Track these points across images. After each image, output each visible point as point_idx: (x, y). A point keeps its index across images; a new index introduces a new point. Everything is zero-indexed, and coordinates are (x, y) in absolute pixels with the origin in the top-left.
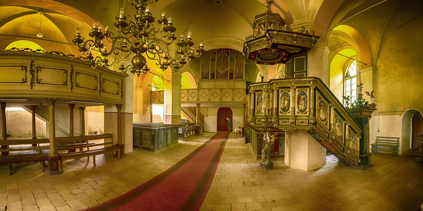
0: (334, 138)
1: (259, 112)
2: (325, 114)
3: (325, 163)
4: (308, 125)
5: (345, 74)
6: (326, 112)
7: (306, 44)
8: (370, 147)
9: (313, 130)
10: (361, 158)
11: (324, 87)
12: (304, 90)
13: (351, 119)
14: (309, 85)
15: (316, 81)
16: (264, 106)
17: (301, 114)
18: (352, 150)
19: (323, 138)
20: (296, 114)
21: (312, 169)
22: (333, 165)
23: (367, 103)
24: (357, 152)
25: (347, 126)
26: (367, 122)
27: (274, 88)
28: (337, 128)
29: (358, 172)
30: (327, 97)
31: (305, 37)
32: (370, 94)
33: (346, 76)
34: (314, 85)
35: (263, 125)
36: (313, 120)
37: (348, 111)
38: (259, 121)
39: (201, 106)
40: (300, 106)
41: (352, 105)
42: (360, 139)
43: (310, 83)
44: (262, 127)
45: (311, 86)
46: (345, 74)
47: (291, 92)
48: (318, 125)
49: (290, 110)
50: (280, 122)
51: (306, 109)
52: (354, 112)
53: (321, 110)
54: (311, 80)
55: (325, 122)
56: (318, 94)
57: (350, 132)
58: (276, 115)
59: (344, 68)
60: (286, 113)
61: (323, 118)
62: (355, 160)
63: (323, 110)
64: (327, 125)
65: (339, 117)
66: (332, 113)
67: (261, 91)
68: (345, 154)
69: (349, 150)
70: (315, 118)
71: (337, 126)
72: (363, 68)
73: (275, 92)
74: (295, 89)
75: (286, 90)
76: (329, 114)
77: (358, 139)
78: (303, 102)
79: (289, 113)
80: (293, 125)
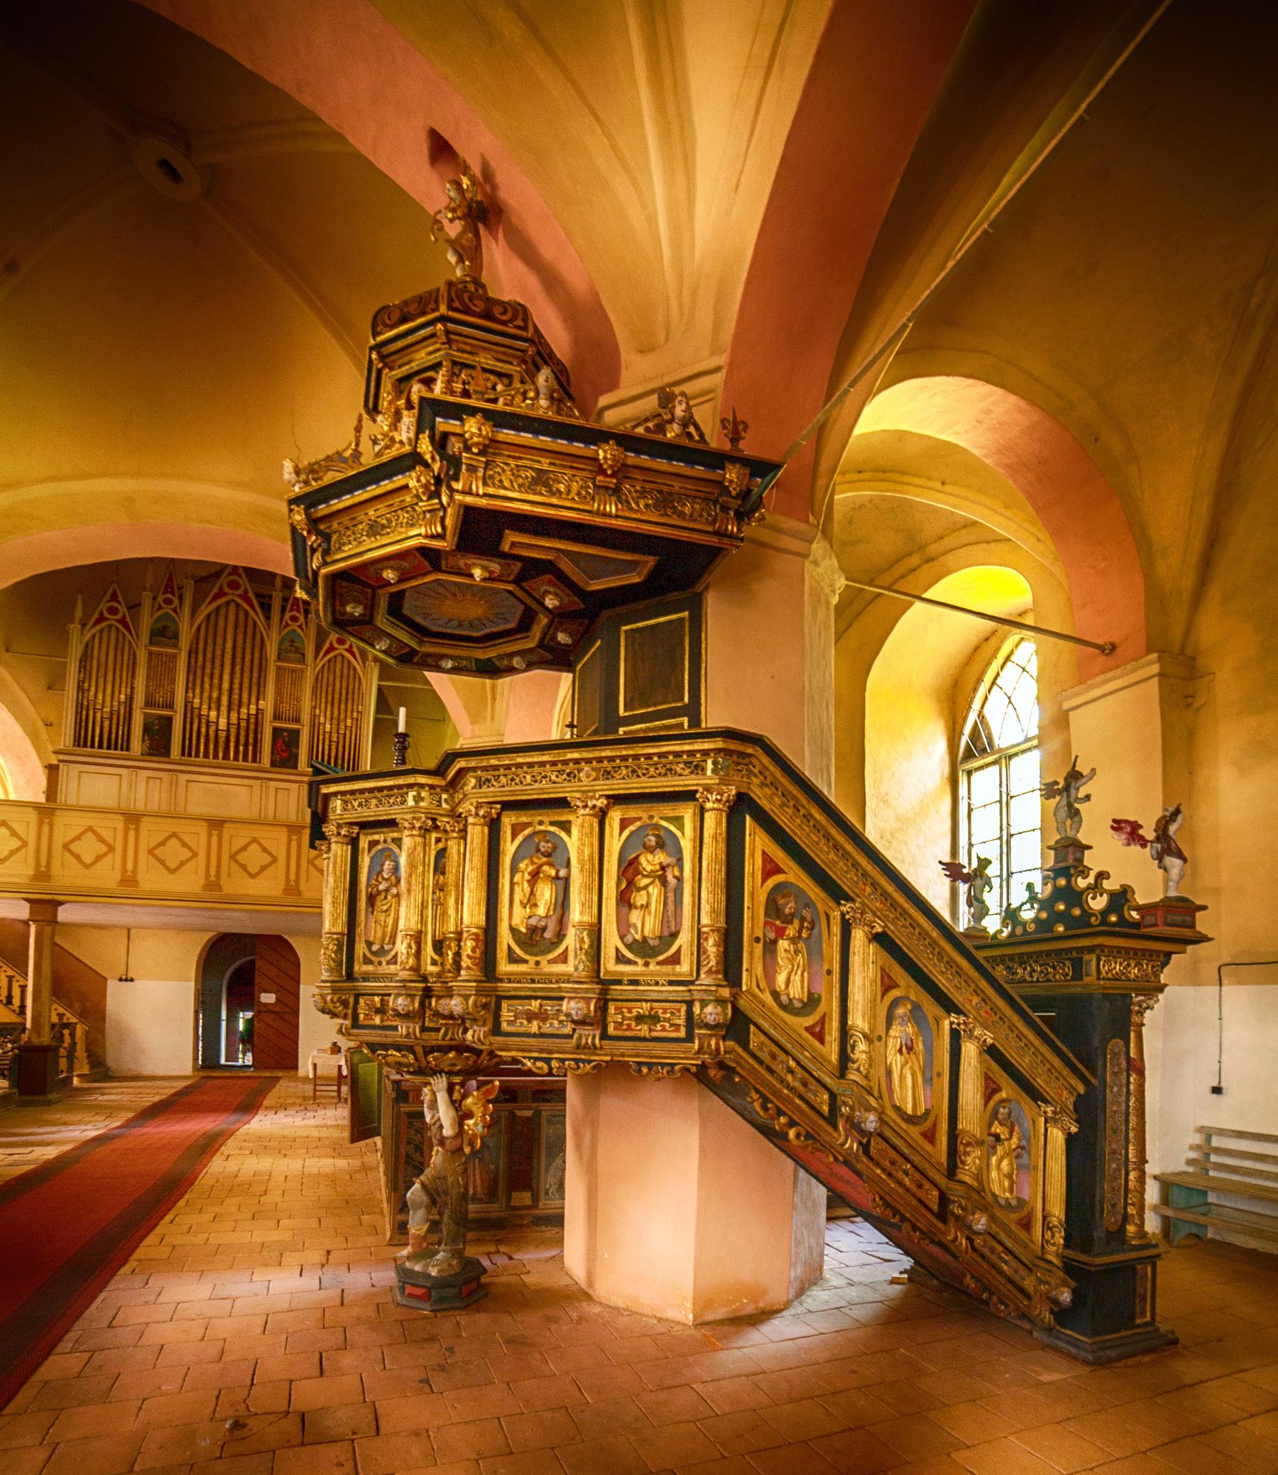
0: (871, 1122)
1: (382, 951)
2: (809, 964)
3: (813, 1277)
4: (690, 1038)
5: (965, 739)
6: (814, 954)
7: (687, 523)
8: (1152, 1193)
9: (721, 1065)
10: (1071, 1269)
11: (802, 798)
12: (660, 814)
13: (1000, 1003)
14: (689, 782)
15: (742, 755)
16: (407, 917)
17: (640, 968)
18: (1008, 1207)
19: (792, 1123)
20: (609, 965)
21: (721, 1313)
22: (871, 1296)
23: (1121, 898)
24: (1046, 1225)
25: (970, 1050)
26: (1123, 1021)
27: (467, 807)
28: (896, 1060)
29: (1054, 1374)
30: (822, 855)
31: (678, 467)
32: (1148, 832)
33: (970, 750)
34: (724, 781)
35: (402, 1030)
36: (720, 1001)
37: (979, 955)
38: (381, 1011)
39: (64, 914)
40: (635, 917)
41: (1011, 915)
42: (1070, 1139)
43: (698, 769)
44: (398, 1048)
45: (708, 789)
46: (965, 739)
47: (575, 831)
48: (755, 1039)
49: (570, 941)
50: (506, 1014)
51: (674, 935)
52: (1023, 960)
53: (783, 944)
54: (706, 753)
55: (809, 1021)
56: (757, 843)
57: (990, 1090)
58: (477, 973)
59: (957, 693)
60: (544, 960)
61: (797, 991)
62: (1029, 1283)
63: (793, 940)
64: (821, 1040)
65: (906, 986)
66: (856, 961)
67: (392, 824)
68: (951, 1233)
69: (984, 1208)
70: (735, 996)
71: (893, 1044)
72: (1083, 677)
73: (477, 833)
74: (602, 815)
75: (543, 821)
76: (836, 967)
77: (1057, 1137)
78: (655, 890)
79: (563, 958)
80: (590, 1035)
